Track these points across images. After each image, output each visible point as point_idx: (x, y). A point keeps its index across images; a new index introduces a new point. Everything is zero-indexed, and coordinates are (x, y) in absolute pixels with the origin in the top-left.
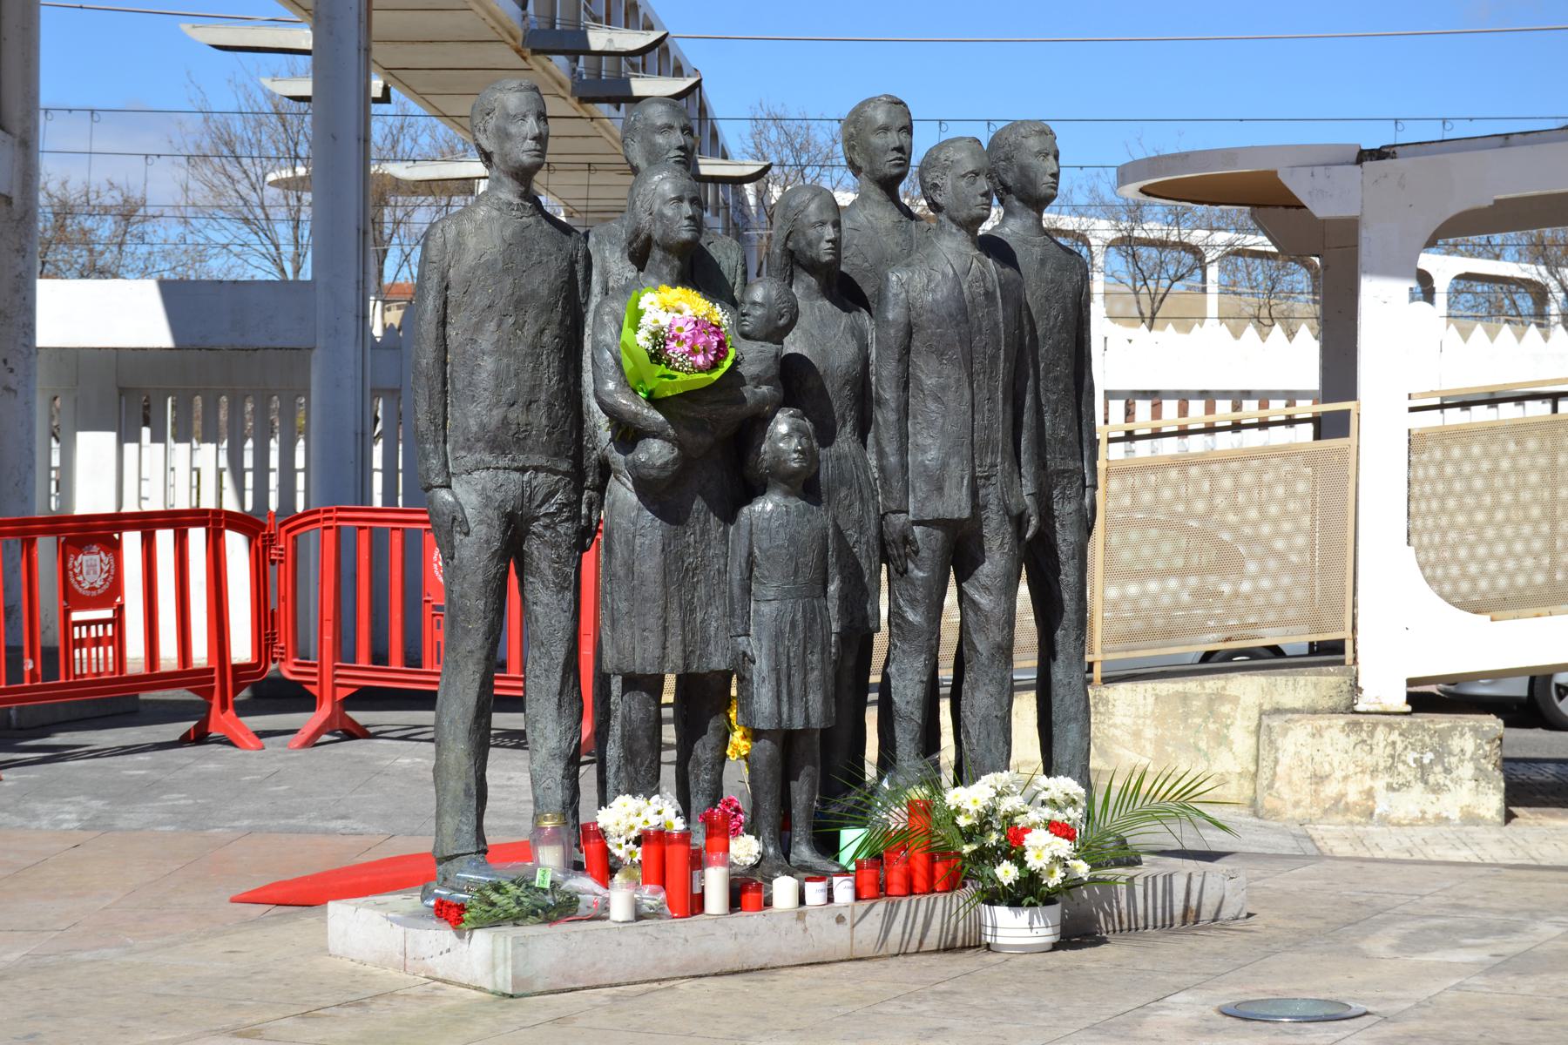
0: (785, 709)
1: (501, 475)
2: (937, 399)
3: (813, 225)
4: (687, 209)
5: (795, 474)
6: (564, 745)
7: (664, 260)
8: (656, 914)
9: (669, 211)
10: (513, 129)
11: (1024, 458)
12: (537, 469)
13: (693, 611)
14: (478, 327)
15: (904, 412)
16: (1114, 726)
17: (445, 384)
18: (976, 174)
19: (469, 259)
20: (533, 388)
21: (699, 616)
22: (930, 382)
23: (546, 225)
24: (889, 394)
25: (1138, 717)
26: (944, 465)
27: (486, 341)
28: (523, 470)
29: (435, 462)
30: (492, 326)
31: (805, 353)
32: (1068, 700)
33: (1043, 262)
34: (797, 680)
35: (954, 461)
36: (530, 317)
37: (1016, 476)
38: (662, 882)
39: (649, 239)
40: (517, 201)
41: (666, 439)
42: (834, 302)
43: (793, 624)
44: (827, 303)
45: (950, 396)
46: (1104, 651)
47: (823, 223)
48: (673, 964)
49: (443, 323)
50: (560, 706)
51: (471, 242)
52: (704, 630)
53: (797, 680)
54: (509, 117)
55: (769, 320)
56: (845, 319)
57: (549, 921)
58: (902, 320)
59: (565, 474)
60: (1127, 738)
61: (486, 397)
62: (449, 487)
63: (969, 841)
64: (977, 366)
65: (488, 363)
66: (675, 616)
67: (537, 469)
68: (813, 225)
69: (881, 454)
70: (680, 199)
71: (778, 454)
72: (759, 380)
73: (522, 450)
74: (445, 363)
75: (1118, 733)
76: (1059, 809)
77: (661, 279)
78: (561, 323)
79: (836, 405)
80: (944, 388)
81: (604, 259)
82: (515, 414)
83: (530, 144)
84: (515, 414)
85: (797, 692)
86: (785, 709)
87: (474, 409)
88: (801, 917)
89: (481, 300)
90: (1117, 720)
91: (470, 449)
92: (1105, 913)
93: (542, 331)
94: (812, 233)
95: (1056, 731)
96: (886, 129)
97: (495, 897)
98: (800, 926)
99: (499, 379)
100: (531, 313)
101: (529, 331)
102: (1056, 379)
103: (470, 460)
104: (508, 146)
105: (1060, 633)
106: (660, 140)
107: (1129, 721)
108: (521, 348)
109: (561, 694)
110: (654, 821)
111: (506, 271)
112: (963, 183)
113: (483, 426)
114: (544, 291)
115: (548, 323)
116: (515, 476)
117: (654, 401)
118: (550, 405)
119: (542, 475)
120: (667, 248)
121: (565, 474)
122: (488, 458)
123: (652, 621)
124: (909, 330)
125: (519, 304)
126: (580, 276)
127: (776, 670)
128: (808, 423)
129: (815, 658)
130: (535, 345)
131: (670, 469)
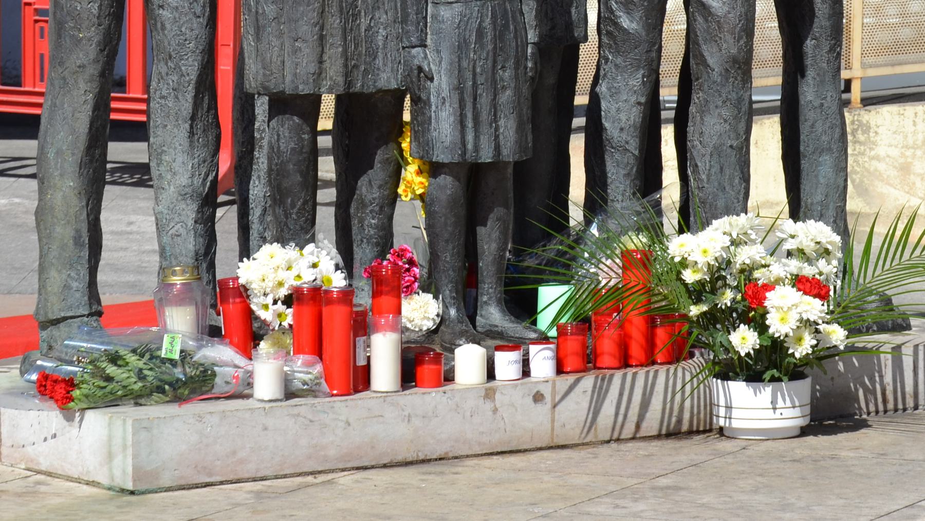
0: (470, 137)
6: (197, 181)
8: (310, 391)
13: (356, 16)
16: (877, 158)
21: (364, 22)
25: (907, 147)
32: (819, 127)
34: (485, 101)
38: (318, 351)
43: (480, 33)
46: (864, 66)
48: (332, 452)
50: (192, 133)
52: (370, 40)
53: (485, 101)
57: (179, 399)
60: (893, 173)
63: (698, 301)
66: (334, 22)
75: (881, 166)
76: (809, 261)
85: (484, 116)
86: (470, 137)
88: (489, 394)
90: (881, 151)
92: (866, 391)
95: (804, 164)
97: (111, 370)
98: (489, 406)
105: (809, 44)
107: (894, 152)
109: (193, 118)
110: (308, 276)
123: (306, 29)
127: (459, 89)
129: (508, 74)
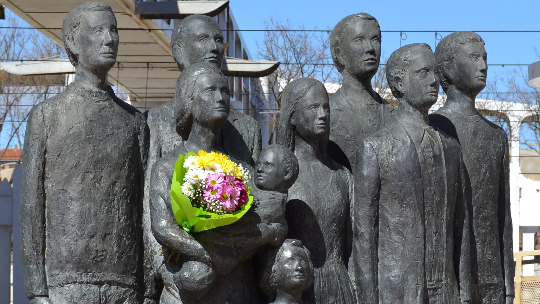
1: (85, 287)
2: (399, 233)
3: (309, 107)
4: (218, 95)
5: (297, 286)
7: (202, 132)
9: (205, 97)
10: (93, 38)
11: (461, 275)
12: (110, 283)
14: (68, 180)
15: (375, 242)
17: (44, 222)
18: (427, 70)
19: (61, 132)
20: (107, 225)
22: (393, 220)
23: (117, 107)
24: (364, 229)
26: (404, 280)
27: (73, 191)
28: (100, 284)
29: (36, 278)
30: (78, 180)
31: (303, 199)
33: (475, 134)
35: (411, 277)
36: (105, 173)
37: (456, 289)
39: (191, 117)
40: (96, 89)
41: (204, 261)
42: (324, 162)
44: (319, 163)
45: (408, 231)
47: (317, 106)
49: (43, 177)
51: (63, 119)
54: (90, 29)
55: (277, 175)
56: (332, 175)
58: (374, 175)
59: (131, 287)
61: (73, 231)
62: (47, 296)
64: (427, 209)
65: (75, 207)
67: (110, 283)
68: (309, 107)
69: (358, 272)
70: (213, 88)
71: (284, 273)
72: (270, 219)
73: (99, 270)
74: (44, 207)
77: (200, 146)
78: (128, 177)
79: (326, 237)
80: (404, 225)
81: (158, 132)
82: (95, 244)
83: (105, 49)
84: (95, 244)
87: (65, 240)
89: (70, 161)
91: (62, 269)
93: (114, 184)
94: (309, 113)
96: (362, 37)
99: (83, 217)
100: (106, 170)
101: (105, 183)
102: (485, 219)
103: (62, 276)
104: (89, 50)
106: (199, 45)
108: (99, 196)
111: (88, 140)
112: (418, 77)
113: (71, 252)
114: (115, 155)
115: (119, 177)
116: (95, 288)
117: (194, 234)
118: (120, 237)
119: (113, 288)
120: (204, 124)
121: (131, 287)
122: (75, 275)
124: (379, 183)
125: (97, 164)
126: (141, 144)
128: (306, 250)
130: (109, 193)
131: (206, 283)
